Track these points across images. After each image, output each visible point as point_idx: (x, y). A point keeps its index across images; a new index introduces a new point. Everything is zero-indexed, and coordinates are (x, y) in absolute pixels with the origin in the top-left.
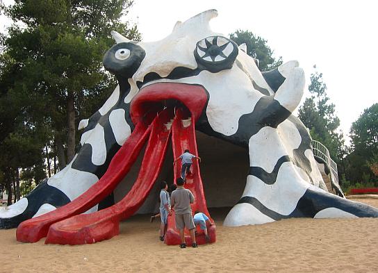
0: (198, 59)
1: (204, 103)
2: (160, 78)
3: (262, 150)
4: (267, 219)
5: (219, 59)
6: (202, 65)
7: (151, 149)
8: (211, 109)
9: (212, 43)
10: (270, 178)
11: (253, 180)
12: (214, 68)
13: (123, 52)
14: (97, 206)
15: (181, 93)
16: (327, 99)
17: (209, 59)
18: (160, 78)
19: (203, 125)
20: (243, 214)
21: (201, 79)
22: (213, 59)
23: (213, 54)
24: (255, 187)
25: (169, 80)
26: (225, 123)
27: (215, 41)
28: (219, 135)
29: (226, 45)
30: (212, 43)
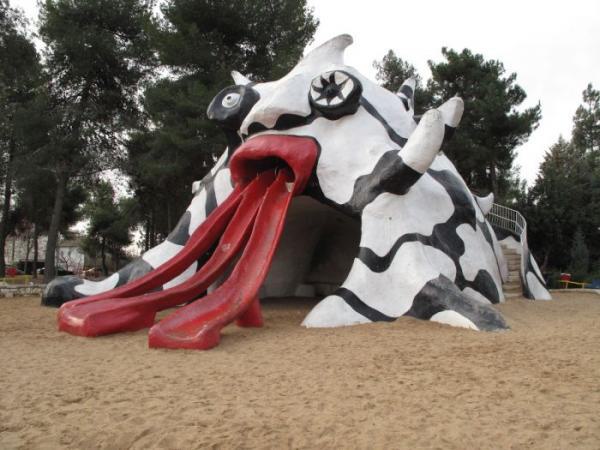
0: (312, 103)
1: (313, 162)
2: (263, 128)
3: (378, 227)
4: (363, 319)
5: (336, 101)
6: (317, 111)
7: (241, 217)
8: (323, 168)
9: (328, 80)
10: (379, 264)
11: (359, 269)
12: (334, 114)
13: (229, 98)
14: (195, 265)
15: (284, 149)
16: (460, 426)
17: (323, 102)
18: (265, 129)
19: (311, 186)
20: (330, 312)
21: (314, 129)
22: (341, 97)
23: (331, 95)
24: (359, 276)
25: (275, 132)
26: (339, 191)
27: (332, 77)
28: (330, 203)
29: (345, 82)
30: (328, 80)
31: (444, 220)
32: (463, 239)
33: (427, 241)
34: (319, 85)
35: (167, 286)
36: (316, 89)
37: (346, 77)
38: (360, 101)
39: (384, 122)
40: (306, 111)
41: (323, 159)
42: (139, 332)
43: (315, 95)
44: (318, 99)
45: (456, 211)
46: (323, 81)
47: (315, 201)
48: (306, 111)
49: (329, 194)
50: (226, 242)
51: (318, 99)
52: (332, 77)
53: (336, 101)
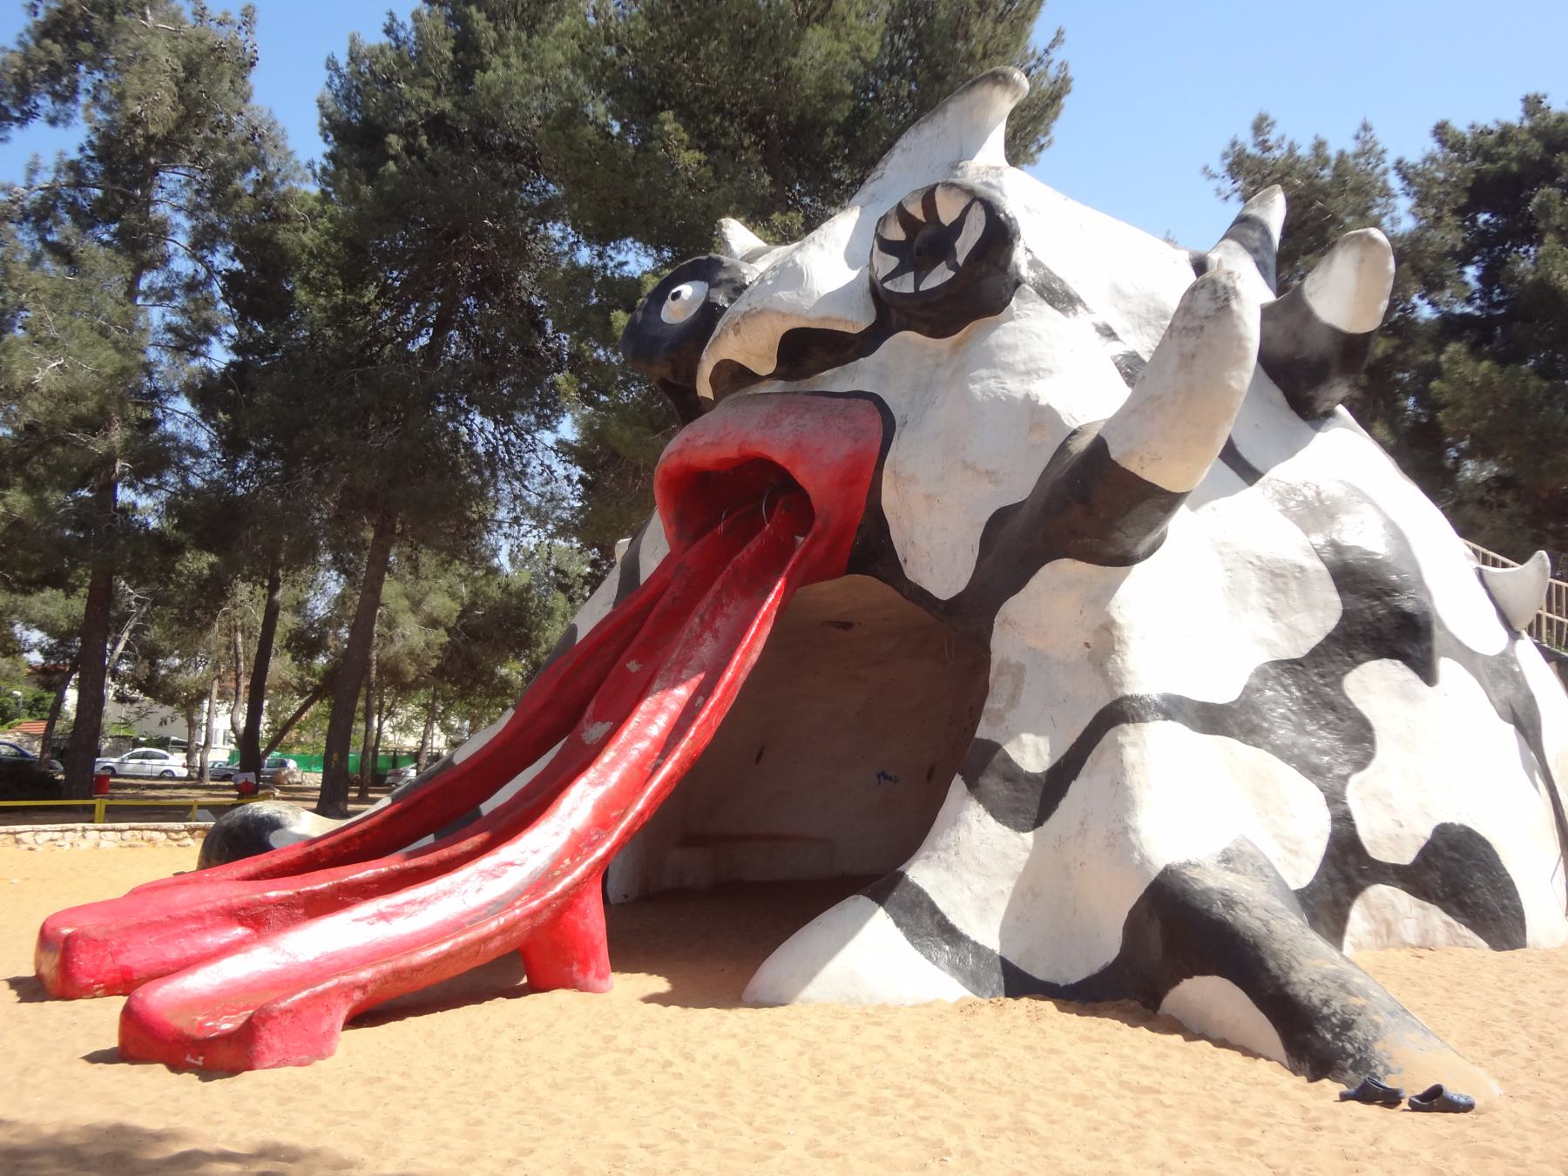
5: (940, 276)
17: (906, 285)
36: (886, 246)
44: (890, 277)
48: (857, 320)
53: (940, 276)
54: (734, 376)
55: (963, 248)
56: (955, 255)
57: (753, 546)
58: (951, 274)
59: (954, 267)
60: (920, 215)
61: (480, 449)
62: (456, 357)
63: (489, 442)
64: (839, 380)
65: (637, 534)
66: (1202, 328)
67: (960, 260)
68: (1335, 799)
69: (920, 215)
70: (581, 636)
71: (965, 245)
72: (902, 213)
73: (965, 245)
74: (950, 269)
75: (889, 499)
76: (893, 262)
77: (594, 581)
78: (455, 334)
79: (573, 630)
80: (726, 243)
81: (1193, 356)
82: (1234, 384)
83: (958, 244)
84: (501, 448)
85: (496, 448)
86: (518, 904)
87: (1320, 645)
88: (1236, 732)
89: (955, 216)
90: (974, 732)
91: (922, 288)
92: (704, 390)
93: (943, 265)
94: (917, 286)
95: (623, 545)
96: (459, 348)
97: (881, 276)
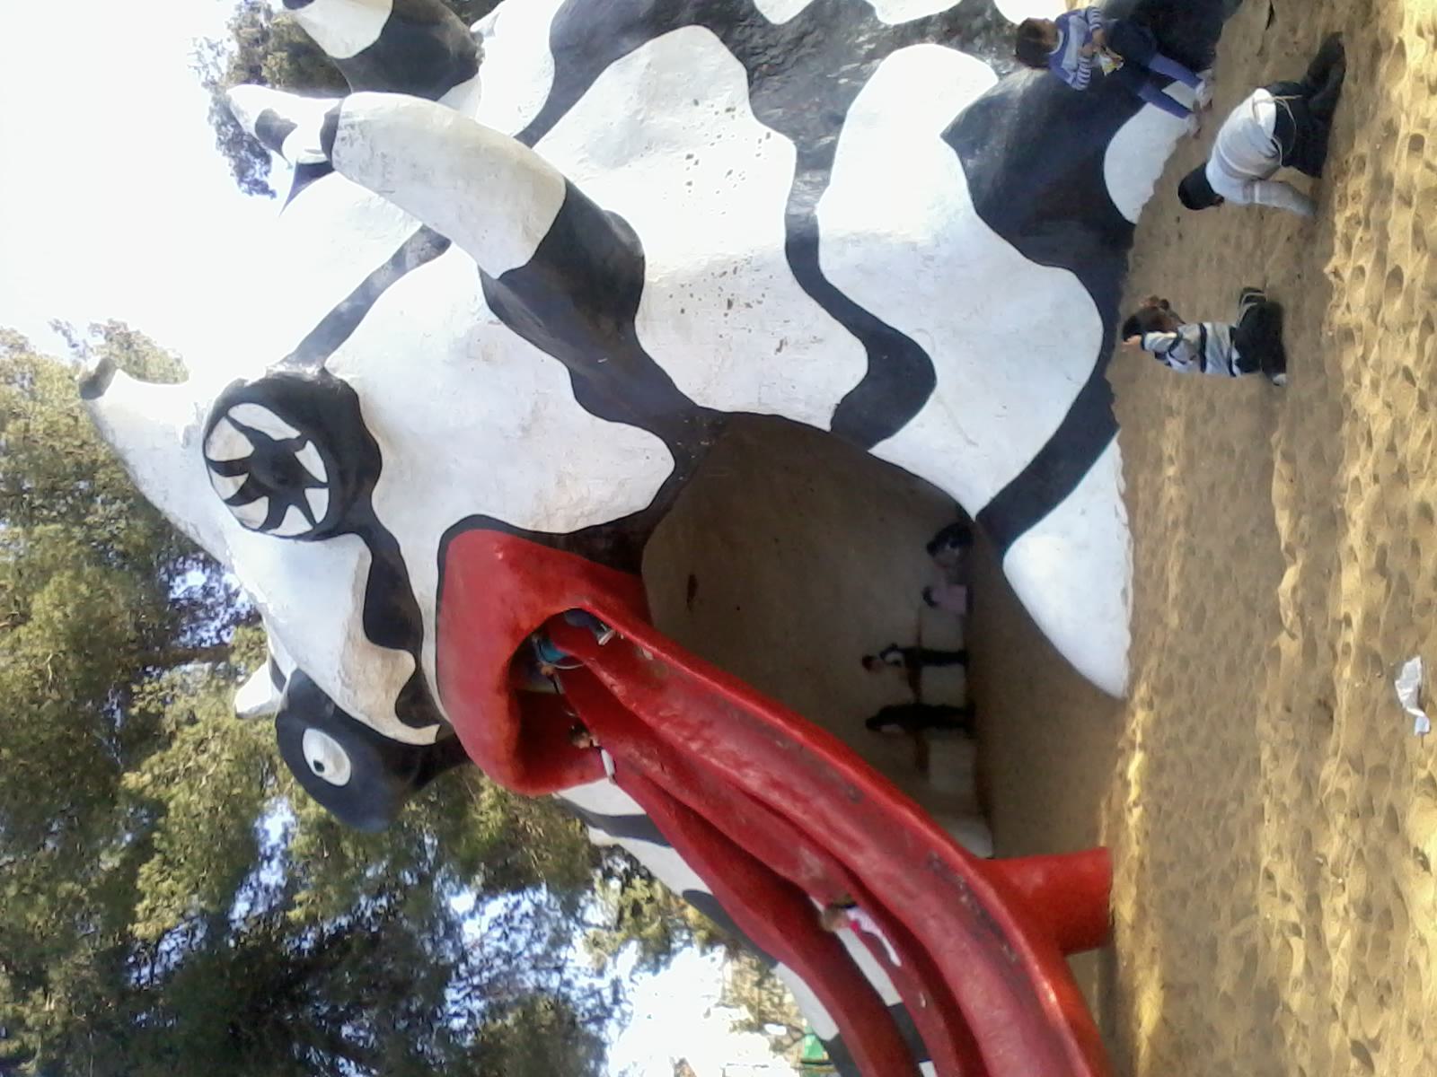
0: (323, 532)
4: (1106, 470)
5: (311, 459)
17: (319, 500)
27: (227, 468)
28: (666, 493)
31: (736, 72)
32: (1178, 198)
33: (815, 161)
34: (259, 509)
35: (891, 996)
36: (273, 521)
37: (225, 427)
38: (311, 371)
39: (399, 263)
40: (352, 555)
41: (522, 516)
42: (937, 960)
43: (294, 520)
44: (309, 515)
45: (699, 20)
46: (243, 497)
47: (660, 530)
48: (352, 555)
49: (639, 498)
50: (794, 863)
51: (309, 515)
52: (227, 468)
53: (311, 459)
54: (413, 703)
55: (279, 430)
56: (287, 440)
57: (607, 678)
58: (310, 446)
59: (300, 442)
60: (241, 479)
61: (477, 1005)
62: (369, 1030)
63: (469, 995)
64: (423, 581)
65: (588, 819)
66: (384, 156)
67: (293, 433)
68: (915, 32)
69: (241, 479)
70: (700, 885)
71: (278, 428)
72: (242, 497)
73: (278, 428)
74: (303, 446)
75: (560, 525)
76: (293, 513)
77: (636, 869)
78: (347, 1030)
79: (692, 896)
80: (270, 703)
81: (414, 166)
82: (448, 122)
83: (276, 436)
84: (476, 980)
85: (475, 987)
86: (274, 919)
87: (732, 50)
88: (827, 140)
89: (243, 439)
90: (824, 431)
91: (322, 477)
92: (425, 736)
93: (299, 455)
94: (321, 485)
95: (599, 837)
96: (361, 1027)
97: (307, 527)
